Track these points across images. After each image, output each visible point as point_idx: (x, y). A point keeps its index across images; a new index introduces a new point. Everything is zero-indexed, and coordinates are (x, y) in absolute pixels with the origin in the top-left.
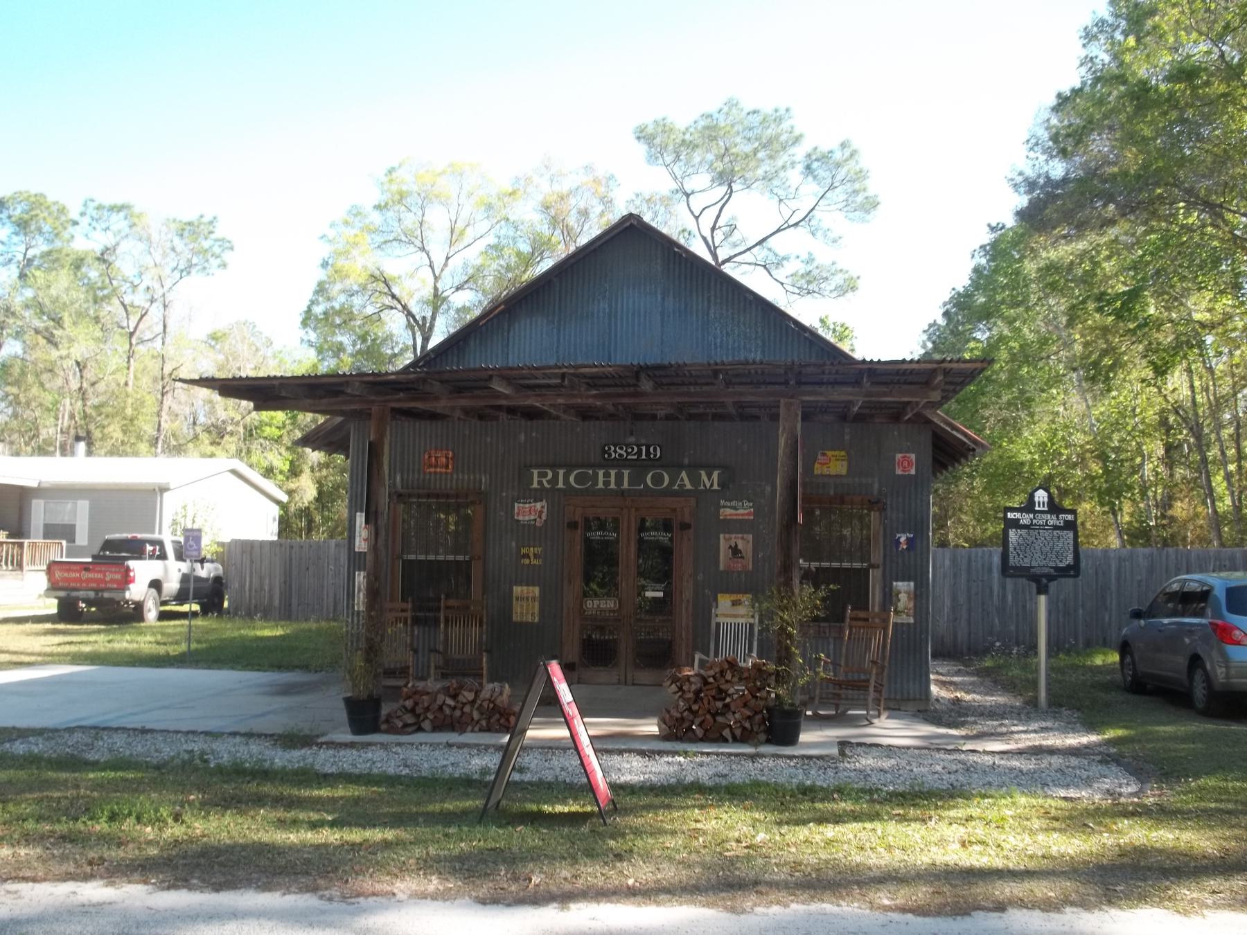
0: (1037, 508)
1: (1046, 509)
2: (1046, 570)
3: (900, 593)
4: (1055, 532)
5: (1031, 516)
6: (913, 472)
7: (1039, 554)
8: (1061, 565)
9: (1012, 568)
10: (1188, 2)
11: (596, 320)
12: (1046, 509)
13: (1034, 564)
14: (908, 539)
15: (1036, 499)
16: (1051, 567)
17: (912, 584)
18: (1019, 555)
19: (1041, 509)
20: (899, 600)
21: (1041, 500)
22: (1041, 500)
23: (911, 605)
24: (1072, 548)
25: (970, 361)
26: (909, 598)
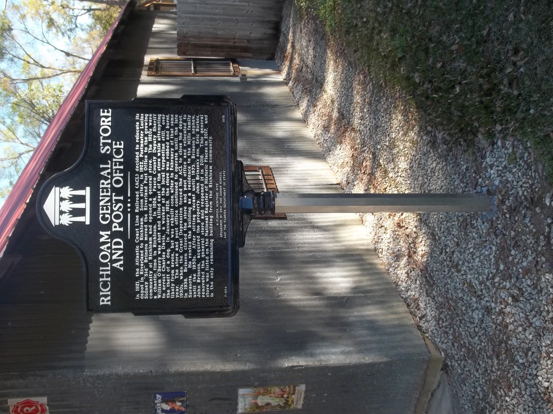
0: (86, 219)
1: (87, 192)
2: (223, 192)
3: (256, 403)
4: (140, 167)
5: (104, 235)
6: (43, 400)
7: (186, 213)
8: (209, 154)
9: (217, 290)
10: (525, 2)
11: (202, 6)
12: (87, 192)
13: (208, 229)
14: (164, 401)
15: (66, 220)
16: (215, 179)
17: (241, 391)
18: (191, 272)
19: (87, 205)
20: (268, 404)
21: (67, 206)
22: (67, 206)
23: (277, 390)
24: (173, 119)
25: (58, 112)
26: (267, 393)
